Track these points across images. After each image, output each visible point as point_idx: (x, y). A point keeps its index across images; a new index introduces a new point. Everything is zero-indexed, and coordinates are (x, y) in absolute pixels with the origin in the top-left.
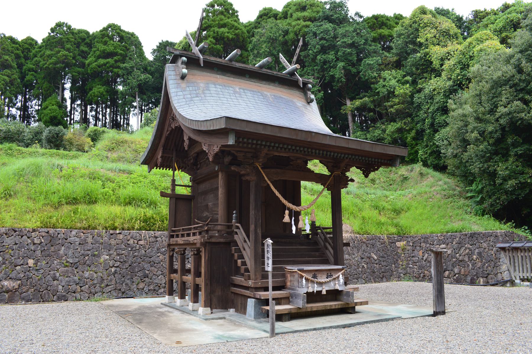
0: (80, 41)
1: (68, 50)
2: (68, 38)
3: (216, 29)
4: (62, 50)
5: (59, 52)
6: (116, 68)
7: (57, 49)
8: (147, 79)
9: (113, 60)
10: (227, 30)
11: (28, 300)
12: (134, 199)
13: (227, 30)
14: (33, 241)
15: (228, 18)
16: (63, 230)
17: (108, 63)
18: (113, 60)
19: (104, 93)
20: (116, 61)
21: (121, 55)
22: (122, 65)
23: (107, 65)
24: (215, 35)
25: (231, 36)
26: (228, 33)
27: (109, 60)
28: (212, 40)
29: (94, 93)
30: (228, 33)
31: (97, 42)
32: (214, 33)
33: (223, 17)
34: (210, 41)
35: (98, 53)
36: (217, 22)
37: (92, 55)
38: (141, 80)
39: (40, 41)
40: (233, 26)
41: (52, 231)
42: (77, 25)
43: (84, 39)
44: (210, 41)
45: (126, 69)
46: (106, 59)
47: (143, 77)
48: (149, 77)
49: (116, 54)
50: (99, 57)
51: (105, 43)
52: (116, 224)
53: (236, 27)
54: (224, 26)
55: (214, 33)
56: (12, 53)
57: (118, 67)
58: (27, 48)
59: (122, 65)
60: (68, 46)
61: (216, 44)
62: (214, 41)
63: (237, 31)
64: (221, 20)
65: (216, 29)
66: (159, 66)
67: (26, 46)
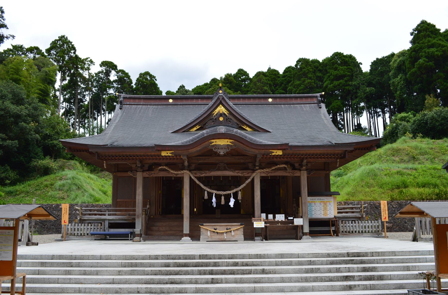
0: (315, 69)
1: (310, 78)
2: (308, 70)
3: (427, 50)
4: (306, 79)
5: (304, 81)
6: (347, 86)
7: (303, 79)
8: (371, 91)
9: (343, 81)
10: (436, 50)
11: (396, 231)
12: (426, 184)
13: (436, 50)
14: (393, 206)
15: (434, 38)
16: (404, 201)
17: (340, 83)
18: (343, 81)
19: (341, 105)
20: (346, 81)
21: (349, 76)
22: (350, 83)
23: (341, 85)
24: (427, 54)
25: (440, 54)
26: (437, 51)
27: (341, 81)
28: (425, 59)
29: (334, 106)
30: (437, 51)
31: (329, 69)
32: (426, 53)
33: (430, 39)
34: (424, 60)
35: (332, 77)
36: (426, 44)
37: (327, 79)
38: (367, 92)
39: (281, 72)
40: (440, 44)
41: (399, 202)
42: (311, 57)
43: (317, 67)
44: (424, 60)
45: (355, 85)
46: (338, 80)
47: (368, 89)
48: (373, 90)
49: (345, 76)
50: (332, 81)
51: (336, 69)
52: (424, 197)
53: (442, 45)
54: (433, 46)
55: (426, 53)
56: (267, 84)
57: (349, 85)
58: (274, 78)
59: (350, 83)
60: (310, 75)
61: (428, 62)
62: (427, 60)
63: (444, 49)
64: (429, 41)
65: (427, 50)
66: (378, 80)
67: (273, 76)
